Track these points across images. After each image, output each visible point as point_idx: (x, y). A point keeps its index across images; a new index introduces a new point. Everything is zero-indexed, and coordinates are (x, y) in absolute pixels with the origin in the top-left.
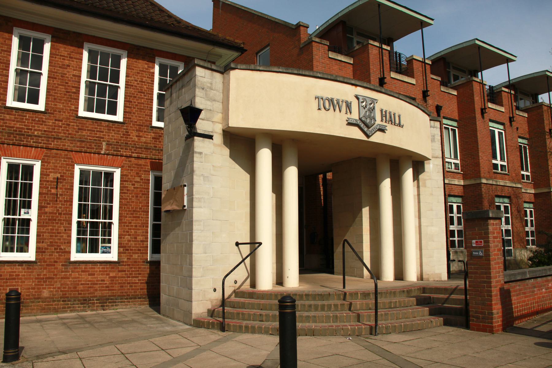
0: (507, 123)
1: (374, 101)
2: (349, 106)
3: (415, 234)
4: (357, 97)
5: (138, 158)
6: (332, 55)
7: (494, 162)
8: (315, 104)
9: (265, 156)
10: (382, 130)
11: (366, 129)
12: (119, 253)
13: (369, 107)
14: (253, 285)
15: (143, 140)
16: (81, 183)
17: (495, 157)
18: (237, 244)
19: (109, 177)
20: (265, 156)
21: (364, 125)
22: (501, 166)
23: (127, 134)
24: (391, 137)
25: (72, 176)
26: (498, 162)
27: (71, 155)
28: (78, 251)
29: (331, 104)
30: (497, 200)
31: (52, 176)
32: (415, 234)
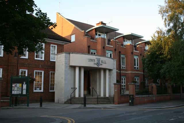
0: (140, 56)
1: (100, 59)
2: (94, 60)
3: (106, 86)
4: (96, 58)
5: (47, 68)
6: (91, 40)
7: (135, 67)
8: (88, 60)
9: (77, 70)
10: (102, 65)
11: (98, 65)
12: (43, 90)
13: (99, 60)
14: (122, 76)
15: (48, 64)
16: (42, 76)
17: (135, 65)
18: (72, 88)
19: (41, 73)
20: (77, 70)
21: (98, 64)
22: (137, 68)
23: (45, 63)
24: (104, 66)
25: (34, 73)
26: (136, 66)
27: (34, 68)
28: (35, 90)
29: (91, 60)
30: (135, 77)
31: (30, 73)
32: (106, 86)
